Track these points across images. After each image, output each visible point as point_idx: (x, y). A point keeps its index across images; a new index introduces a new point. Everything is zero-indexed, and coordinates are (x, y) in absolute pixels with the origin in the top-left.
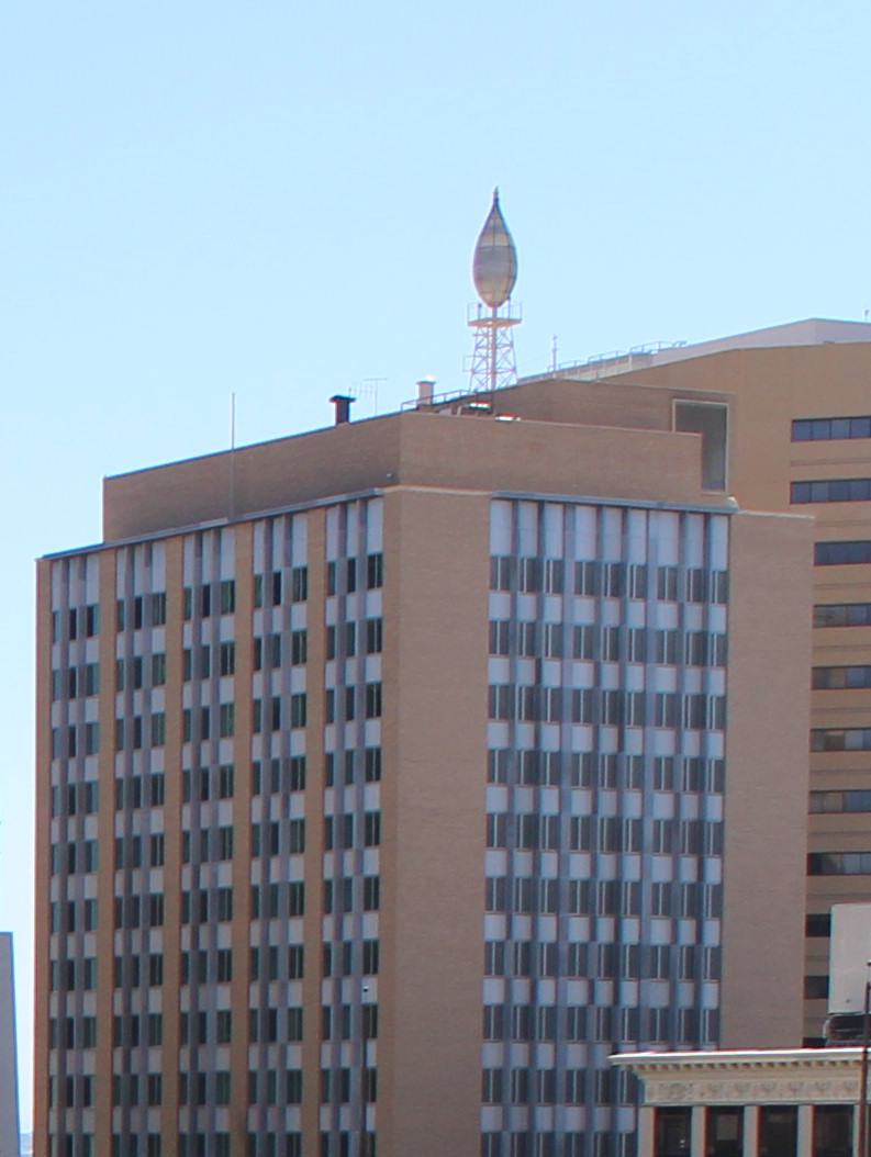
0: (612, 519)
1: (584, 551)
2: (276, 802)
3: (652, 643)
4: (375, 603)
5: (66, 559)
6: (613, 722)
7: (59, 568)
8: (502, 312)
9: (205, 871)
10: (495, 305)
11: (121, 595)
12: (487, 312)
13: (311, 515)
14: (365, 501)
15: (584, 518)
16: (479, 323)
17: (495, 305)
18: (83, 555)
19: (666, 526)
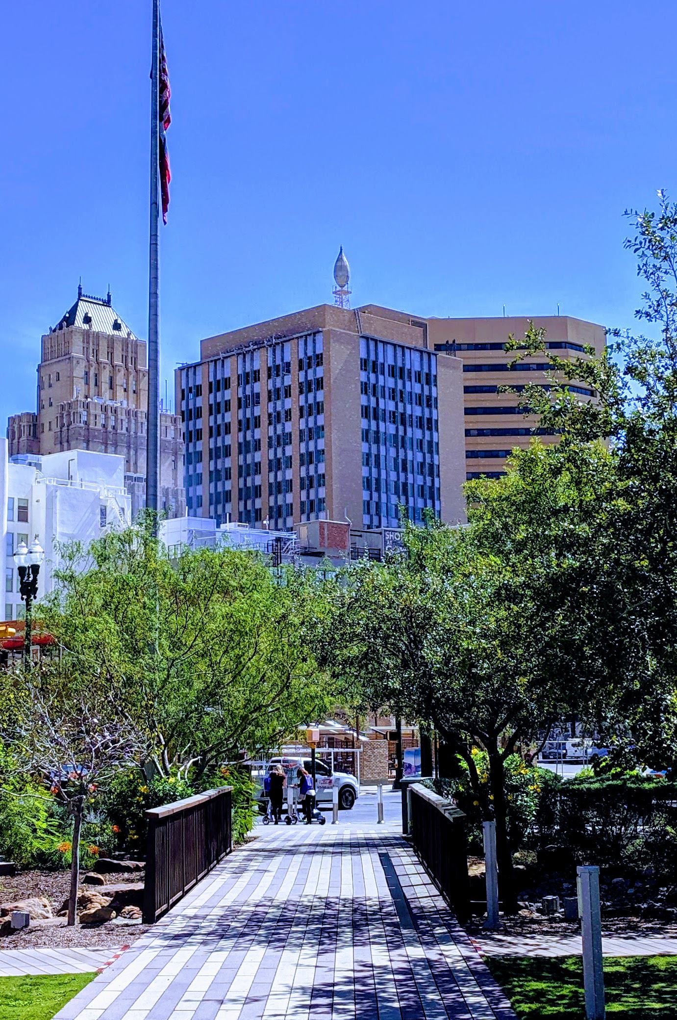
0: (399, 351)
1: (390, 361)
2: (279, 450)
3: (387, 415)
4: (320, 372)
5: (188, 367)
6: (374, 443)
7: (184, 373)
8: (345, 288)
9: (249, 479)
10: (342, 287)
11: (211, 379)
12: (339, 288)
13: (292, 341)
14: (315, 334)
15: (390, 349)
16: (335, 293)
17: (342, 287)
18: (195, 366)
19: (416, 356)
